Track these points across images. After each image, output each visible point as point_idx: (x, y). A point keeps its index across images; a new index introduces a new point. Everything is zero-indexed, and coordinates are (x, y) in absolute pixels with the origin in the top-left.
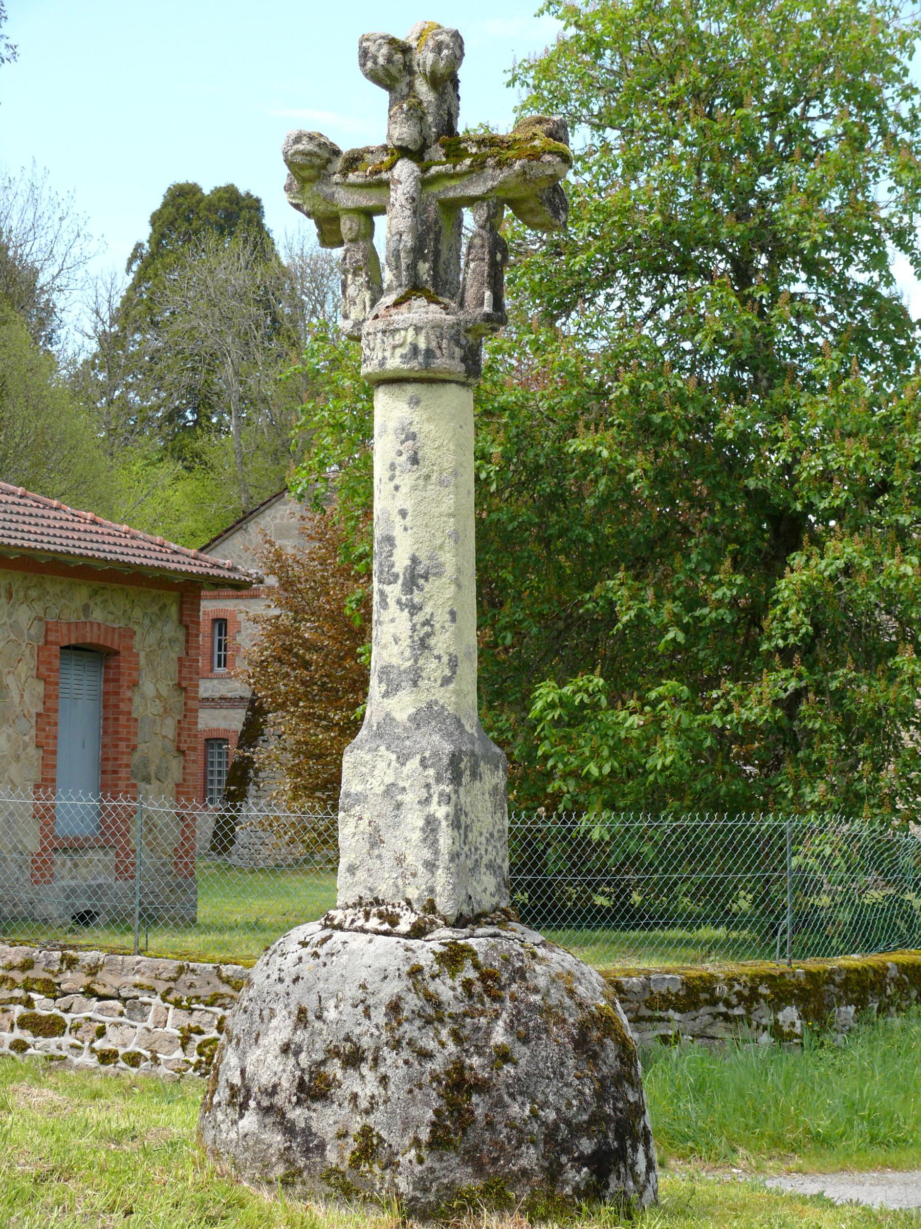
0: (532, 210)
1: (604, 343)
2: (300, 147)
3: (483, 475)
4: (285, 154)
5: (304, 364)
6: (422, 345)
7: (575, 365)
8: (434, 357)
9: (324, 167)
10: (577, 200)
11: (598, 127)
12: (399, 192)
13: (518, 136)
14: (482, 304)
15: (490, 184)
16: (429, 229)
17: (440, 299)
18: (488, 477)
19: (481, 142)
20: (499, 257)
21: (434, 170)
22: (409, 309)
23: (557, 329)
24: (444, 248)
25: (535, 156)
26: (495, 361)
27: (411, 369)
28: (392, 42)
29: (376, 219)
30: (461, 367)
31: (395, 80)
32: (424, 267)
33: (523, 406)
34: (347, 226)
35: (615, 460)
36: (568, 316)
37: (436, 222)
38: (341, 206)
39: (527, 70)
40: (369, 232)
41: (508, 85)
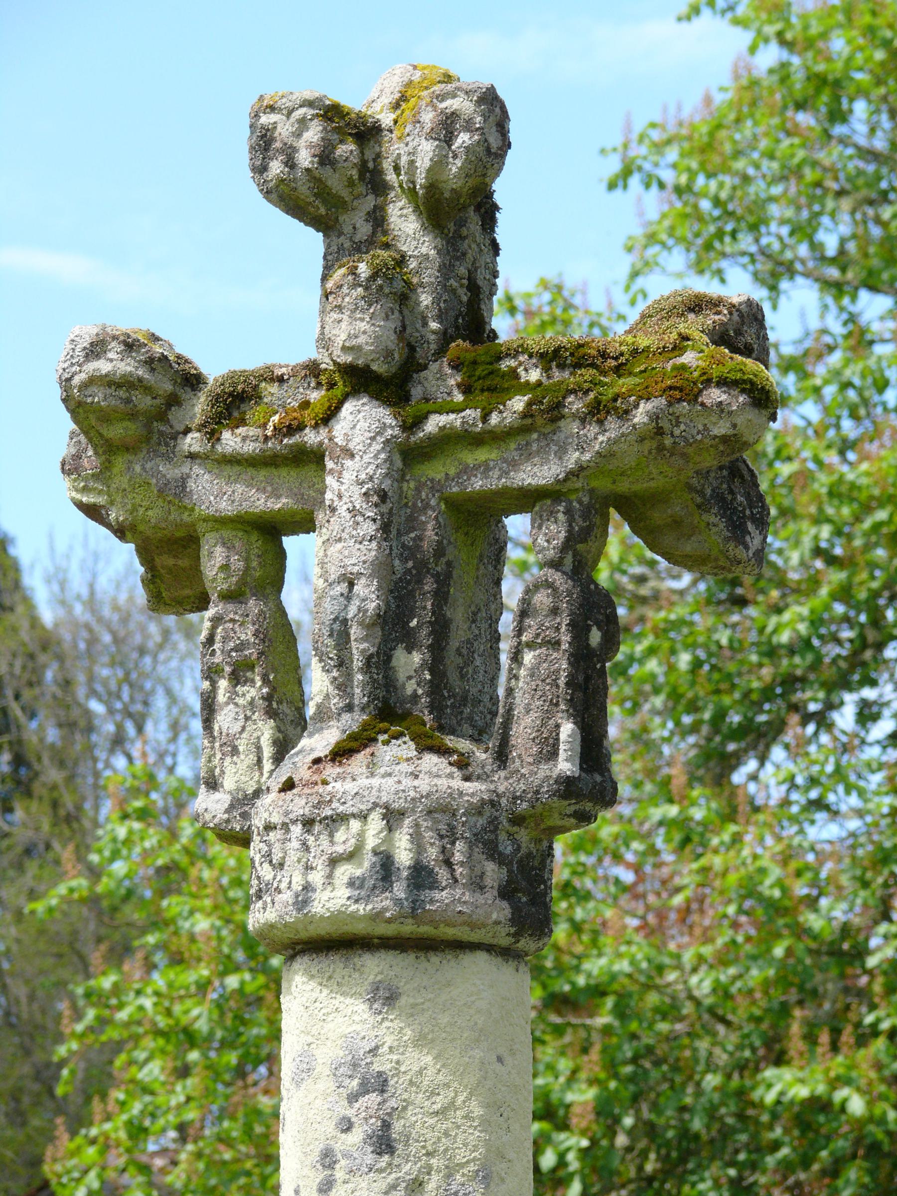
0: (676, 523)
1: (854, 824)
2: (103, 366)
3: (548, 1160)
4: (66, 383)
5: (95, 873)
6: (404, 856)
7: (779, 883)
8: (434, 885)
9: (162, 416)
10: (785, 469)
11: (837, 288)
12: (348, 477)
13: (643, 342)
14: (554, 754)
15: (573, 458)
16: (422, 567)
17: (450, 741)
18: (562, 1162)
19: (551, 358)
20: (595, 637)
21: (434, 424)
22: (372, 767)
23: (734, 790)
24: (458, 615)
25: (685, 390)
26: (580, 871)
27: (376, 917)
28: (332, 113)
29: (290, 543)
30: (502, 911)
31: (338, 204)
32: (410, 663)
33: (648, 987)
34: (216, 561)
35: (882, 1121)
36: (763, 760)
37: (440, 551)
38: (203, 509)
39: (659, 147)
40: (270, 576)
41: (612, 186)
